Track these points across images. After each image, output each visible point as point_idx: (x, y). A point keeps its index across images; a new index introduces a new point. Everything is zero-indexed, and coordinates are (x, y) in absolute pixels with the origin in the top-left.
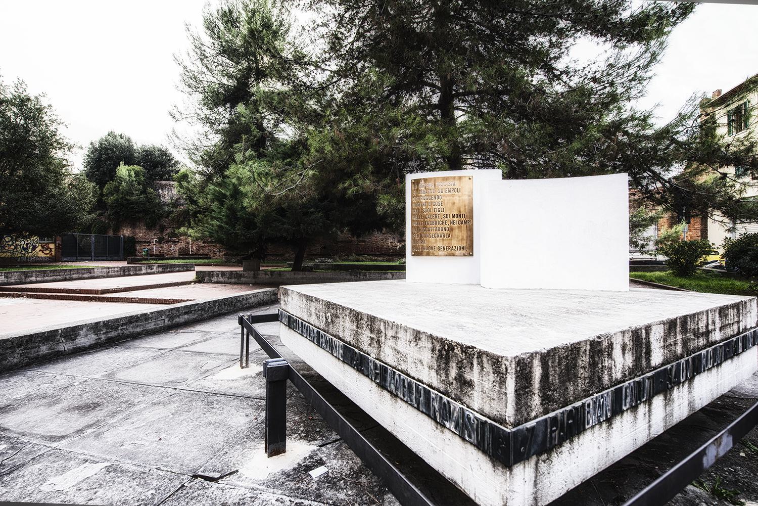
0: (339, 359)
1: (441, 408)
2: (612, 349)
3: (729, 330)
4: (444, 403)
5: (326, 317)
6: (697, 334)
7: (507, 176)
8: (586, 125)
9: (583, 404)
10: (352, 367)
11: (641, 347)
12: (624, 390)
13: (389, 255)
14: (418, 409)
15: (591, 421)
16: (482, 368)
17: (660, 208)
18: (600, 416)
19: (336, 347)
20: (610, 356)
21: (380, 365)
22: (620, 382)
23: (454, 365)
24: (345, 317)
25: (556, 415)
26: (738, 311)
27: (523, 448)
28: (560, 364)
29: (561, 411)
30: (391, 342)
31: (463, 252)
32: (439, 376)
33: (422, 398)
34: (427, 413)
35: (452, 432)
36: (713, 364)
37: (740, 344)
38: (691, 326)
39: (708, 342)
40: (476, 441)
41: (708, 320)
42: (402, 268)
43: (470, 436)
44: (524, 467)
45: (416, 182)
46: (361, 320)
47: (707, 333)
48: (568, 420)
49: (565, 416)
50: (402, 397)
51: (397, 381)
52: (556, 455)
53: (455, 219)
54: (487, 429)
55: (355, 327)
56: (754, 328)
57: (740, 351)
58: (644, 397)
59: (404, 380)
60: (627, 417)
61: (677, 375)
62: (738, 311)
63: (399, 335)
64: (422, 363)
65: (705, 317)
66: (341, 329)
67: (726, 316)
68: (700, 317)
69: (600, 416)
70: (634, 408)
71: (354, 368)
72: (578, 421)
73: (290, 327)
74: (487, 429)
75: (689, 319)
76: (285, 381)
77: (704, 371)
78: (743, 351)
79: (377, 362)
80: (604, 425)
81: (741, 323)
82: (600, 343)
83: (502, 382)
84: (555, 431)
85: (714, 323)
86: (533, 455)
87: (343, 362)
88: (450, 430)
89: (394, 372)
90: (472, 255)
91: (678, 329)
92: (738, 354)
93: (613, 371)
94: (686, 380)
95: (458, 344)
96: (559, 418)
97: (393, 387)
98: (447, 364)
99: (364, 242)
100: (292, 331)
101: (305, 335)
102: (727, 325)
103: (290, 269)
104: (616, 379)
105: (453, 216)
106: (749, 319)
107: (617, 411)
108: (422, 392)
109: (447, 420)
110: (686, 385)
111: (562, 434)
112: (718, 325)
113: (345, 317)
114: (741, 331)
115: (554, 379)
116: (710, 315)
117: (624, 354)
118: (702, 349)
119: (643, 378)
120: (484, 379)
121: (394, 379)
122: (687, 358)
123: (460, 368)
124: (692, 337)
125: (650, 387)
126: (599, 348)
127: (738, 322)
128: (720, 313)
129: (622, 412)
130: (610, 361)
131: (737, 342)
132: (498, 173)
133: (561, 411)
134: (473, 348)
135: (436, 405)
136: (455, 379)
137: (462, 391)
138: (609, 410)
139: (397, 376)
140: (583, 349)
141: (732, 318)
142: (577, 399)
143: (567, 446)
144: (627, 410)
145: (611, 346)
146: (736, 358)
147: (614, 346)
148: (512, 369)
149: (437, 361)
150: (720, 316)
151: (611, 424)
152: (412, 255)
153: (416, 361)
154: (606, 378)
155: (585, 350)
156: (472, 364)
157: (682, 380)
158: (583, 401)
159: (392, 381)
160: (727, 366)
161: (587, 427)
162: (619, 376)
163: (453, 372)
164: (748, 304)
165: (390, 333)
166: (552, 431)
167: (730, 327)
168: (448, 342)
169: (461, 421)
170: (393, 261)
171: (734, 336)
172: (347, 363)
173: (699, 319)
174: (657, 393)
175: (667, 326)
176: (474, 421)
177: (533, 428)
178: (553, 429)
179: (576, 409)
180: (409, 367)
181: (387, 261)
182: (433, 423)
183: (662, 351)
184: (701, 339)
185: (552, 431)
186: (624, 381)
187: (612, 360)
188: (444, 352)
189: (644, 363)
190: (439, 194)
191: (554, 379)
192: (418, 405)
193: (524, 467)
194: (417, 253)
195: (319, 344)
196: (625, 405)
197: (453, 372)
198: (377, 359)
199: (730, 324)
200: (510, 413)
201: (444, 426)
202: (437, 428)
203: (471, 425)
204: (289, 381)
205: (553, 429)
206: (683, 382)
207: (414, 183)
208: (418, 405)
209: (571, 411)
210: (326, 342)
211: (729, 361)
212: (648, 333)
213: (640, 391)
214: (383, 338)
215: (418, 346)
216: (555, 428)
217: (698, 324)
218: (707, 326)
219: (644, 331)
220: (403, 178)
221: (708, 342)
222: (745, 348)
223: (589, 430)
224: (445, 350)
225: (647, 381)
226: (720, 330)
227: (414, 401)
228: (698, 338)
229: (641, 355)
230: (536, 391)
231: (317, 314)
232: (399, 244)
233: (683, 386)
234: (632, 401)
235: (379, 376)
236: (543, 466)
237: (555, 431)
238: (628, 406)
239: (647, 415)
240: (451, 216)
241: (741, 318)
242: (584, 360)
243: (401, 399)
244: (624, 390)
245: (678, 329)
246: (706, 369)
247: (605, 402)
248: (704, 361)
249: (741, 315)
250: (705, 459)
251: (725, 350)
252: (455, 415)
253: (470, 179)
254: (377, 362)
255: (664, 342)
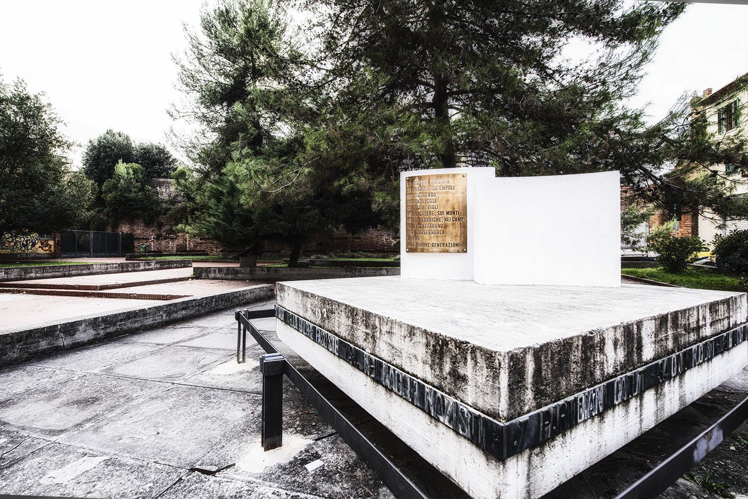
0: (334, 354)
1: (435, 402)
2: (604, 344)
3: (720, 325)
4: (439, 397)
5: (322, 313)
6: (688, 330)
7: (501, 173)
8: (578, 124)
9: (576, 399)
10: (347, 361)
11: (633, 342)
12: (616, 384)
13: (383, 252)
14: (412, 403)
15: (583, 415)
16: (476, 363)
17: (651, 205)
18: (592, 410)
19: (331, 342)
20: (602, 351)
21: (375, 360)
22: (612, 377)
23: (448, 360)
24: (340, 313)
25: (549, 409)
26: (729, 307)
27: (516, 442)
28: (552, 359)
29: (554, 405)
30: (386, 337)
31: (457, 248)
32: (433, 371)
33: (416, 393)
34: (422, 407)
35: (446, 426)
36: (704, 359)
37: (731, 340)
38: (682, 321)
39: (699, 337)
40: (469, 435)
41: (698, 315)
42: (397, 264)
43: (463, 430)
44: (517, 461)
45: (411, 180)
46: (356, 315)
47: (698, 328)
48: (561, 414)
49: (558, 410)
50: (397, 392)
51: (392, 376)
52: (548, 449)
53: (449, 216)
54: (481, 423)
55: (350, 323)
56: (744, 323)
57: (730, 346)
58: (635, 392)
59: (398, 375)
60: (619, 411)
61: (668, 370)
62: (729, 307)
63: (394, 331)
64: (416, 358)
65: (695, 313)
66: (337, 324)
67: (717, 311)
68: (691, 313)
69: (592, 410)
70: (626, 403)
71: (349, 363)
72: (570, 415)
73: (286, 323)
74: (481, 423)
75: (680, 315)
76: (282, 375)
77: (695, 366)
78: (733, 346)
79: (372, 357)
80: (596, 420)
81: (731, 319)
82: (592, 338)
83: (496, 377)
84: (548, 425)
85: (704, 318)
86: (526, 449)
87: (339, 357)
88: (444, 424)
89: (389, 367)
90: (466, 252)
91: (669, 325)
92: (728, 350)
93: (605, 366)
94: (677, 375)
95: (452, 339)
96: (552, 412)
97: (388, 381)
98: (441, 359)
99: (360, 238)
100: (288, 326)
101: (301, 331)
102: (717, 321)
103: (286, 265)
104: (608, 374)
105: (448, 213)
106: (739, 315)
107: (609, 405)
108: (417, 387)
109: (441, 415)
110: (677, 380)
111: (554, 428)
112: (709, 321)
113: (340, 313)
114: (731, 326)
115: (547, 373)
116: (701, 311)
117: (615, 349)
118: (693, 344)
119: (635, 373)
120: (478, 374)
121: (389, 373)
122: (677, 353)
123: (454, 363)
124: (683, 332)
125: (641, 382)
126: (591, 343)
127: (728, 318)
128: (710, 309)
129: (614, 406)
130: (602, 356)
131: (727, 337)
132: (491, 170)
133: (554, 405)
134: (467, 343)
135: (431, 400)
136: (449, 373)
137: (456, 385)
138: (601, 404)
139: (391, 371)
140: (575, 344)
141: (722, 313)
142: (569, 394)
143: (559, 440)
144: (619, 404)
145: (603, 341)
146: (726, 353)
147: (606, 341)
148: (505, 364)
149: (431, 356)
150: (711, 312)
151: (603, 418)
152: (407, 252)
153: (411, 356)
154: (598, 373)
155: (578, 346)
156: (466, 359)
157: (673, 375)
158: (576, 395)
159: (387, 376)
160: (718, 361)
161: (579, 421)
162: (611, 370)
163: (447, 367)
164: (738, 300)
165: (385, 328)
166: (545, 425)
167: (720, 323)
168: (442, 337)
169: (455, 415)
170: (387, 257)
171: (724, 331)
172: (342, 358)
173: (690, 315)
174: (648, 388)
175: (658, 322)
176: (467, 415)
177: (526, 422)
178: (546, 423)
179: (568, 403)
180: (403, 362)
181: (382, 257)
182: (427, 417)
183: (653, 346)
184: (692, 334)
185: (545, 425)
186: (616, 376)
187: (604, 355)
188: (438, 348)
189: (635, 358)
190: (433, 192)
191: (547, 373)
192: (413, 400)
193: (517, 461)
194: (411, 250)
195: (315, 339)
196: (617, 400)
197: (447, 367)
198: (372, 354)
199: (720, 320)
200: (503, 407)
201: (438, 420)
202: (431, 422)
203: (465, 419)
204: (285, 376)
205: (546, 423)
206: (674, 377)
207: (408, 180)
208: (413, 400)
209: (564, 405)
210: (322, 337)
211: (720, 356)
212: (639, 329)
213: (631, 386)
214: (378, 333)
215: (413, 341)
216: (547, 422)
217: (688, 320)
218: (698, 322)
219: (635, 327)
220: (397, 176)
221: (699, 337)
222: (735, 343)
223: (582, 424)
224: (439, 345)
225: (638, 375)
226: (711, 325)
227: (409, 395)
228: (689, 333)
229: (632, 350)
230: (529, 386)
231: (312, 310)
232: (393, 241)
233: (674, 381)
234: (623, 395)
235: (374, 371)
236: (536, 460)
237: (548, 425)
238: (620, 400)
239: (639, 409)
240: (445, 213)
241: (731, 314)
242: (576, 355)
243: (395, 393)
244: (616, 384)
245: (669, 325)
246: (697, 363)
247: (597, 397)
248: (694, 356)
249: (731, 311)
250: (695, 453)
251: (715, 345)
252: (449, 409)
253: (464, 176)
254: (372, 357)
255: (655, 337)
